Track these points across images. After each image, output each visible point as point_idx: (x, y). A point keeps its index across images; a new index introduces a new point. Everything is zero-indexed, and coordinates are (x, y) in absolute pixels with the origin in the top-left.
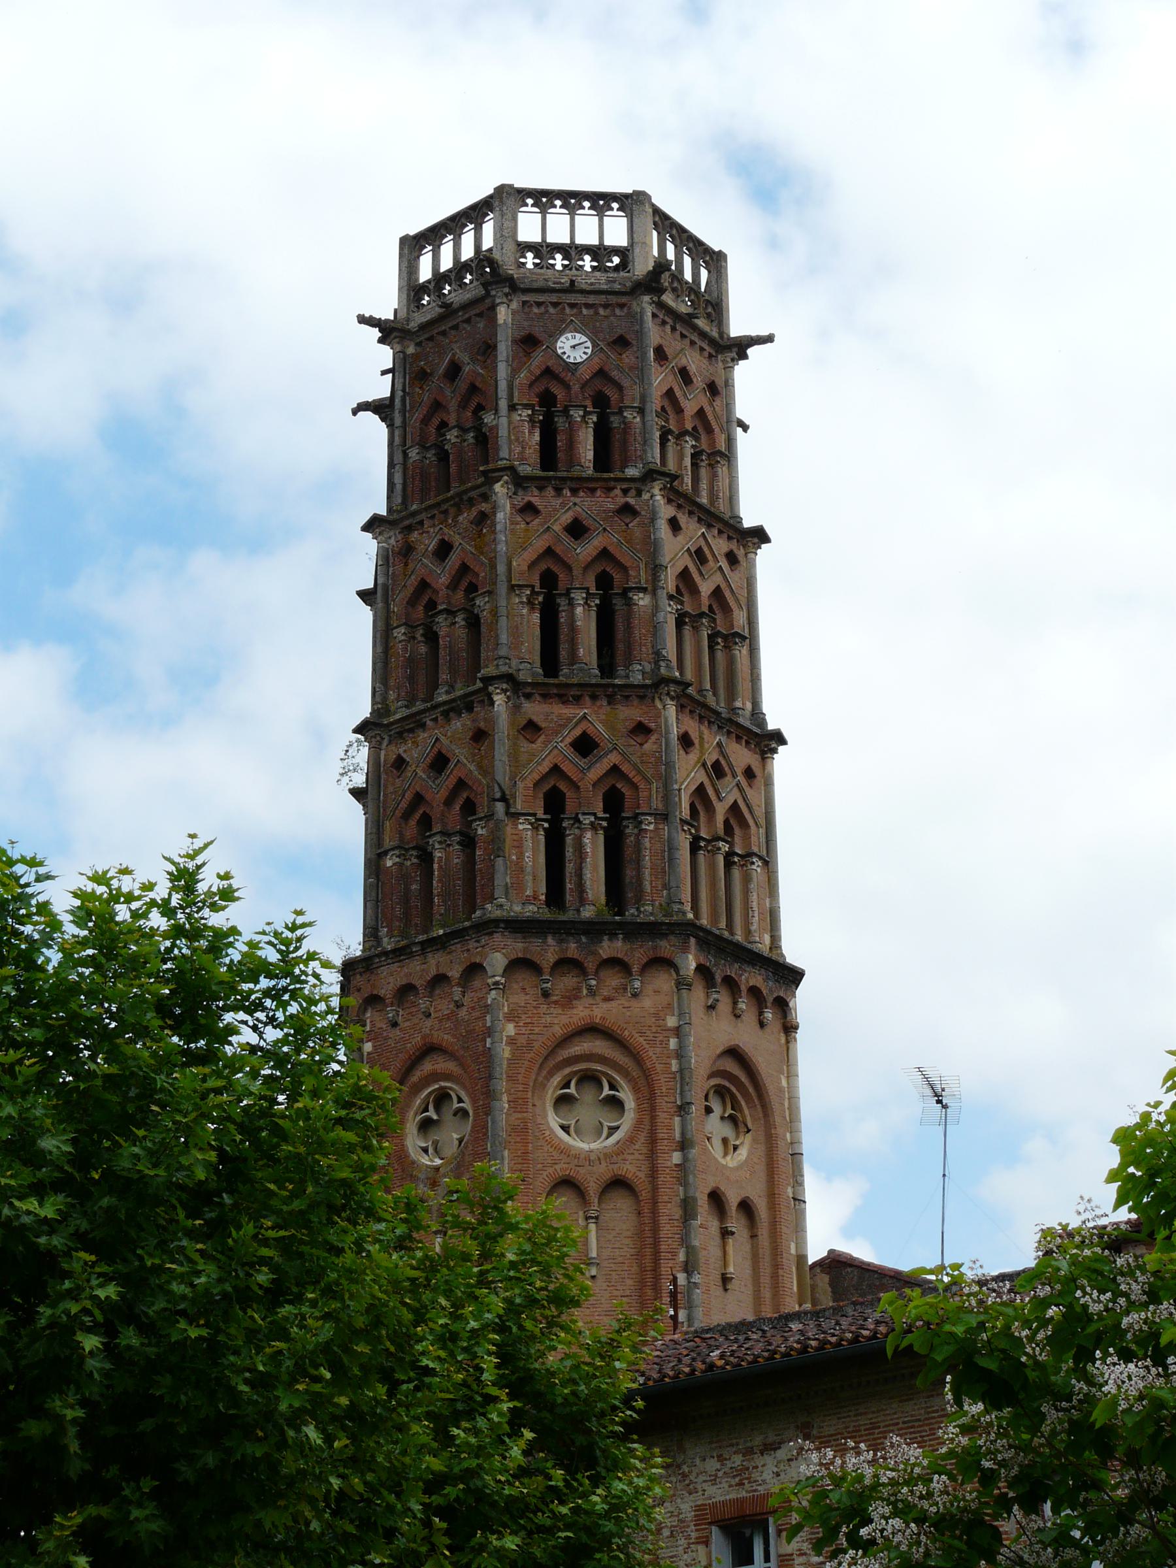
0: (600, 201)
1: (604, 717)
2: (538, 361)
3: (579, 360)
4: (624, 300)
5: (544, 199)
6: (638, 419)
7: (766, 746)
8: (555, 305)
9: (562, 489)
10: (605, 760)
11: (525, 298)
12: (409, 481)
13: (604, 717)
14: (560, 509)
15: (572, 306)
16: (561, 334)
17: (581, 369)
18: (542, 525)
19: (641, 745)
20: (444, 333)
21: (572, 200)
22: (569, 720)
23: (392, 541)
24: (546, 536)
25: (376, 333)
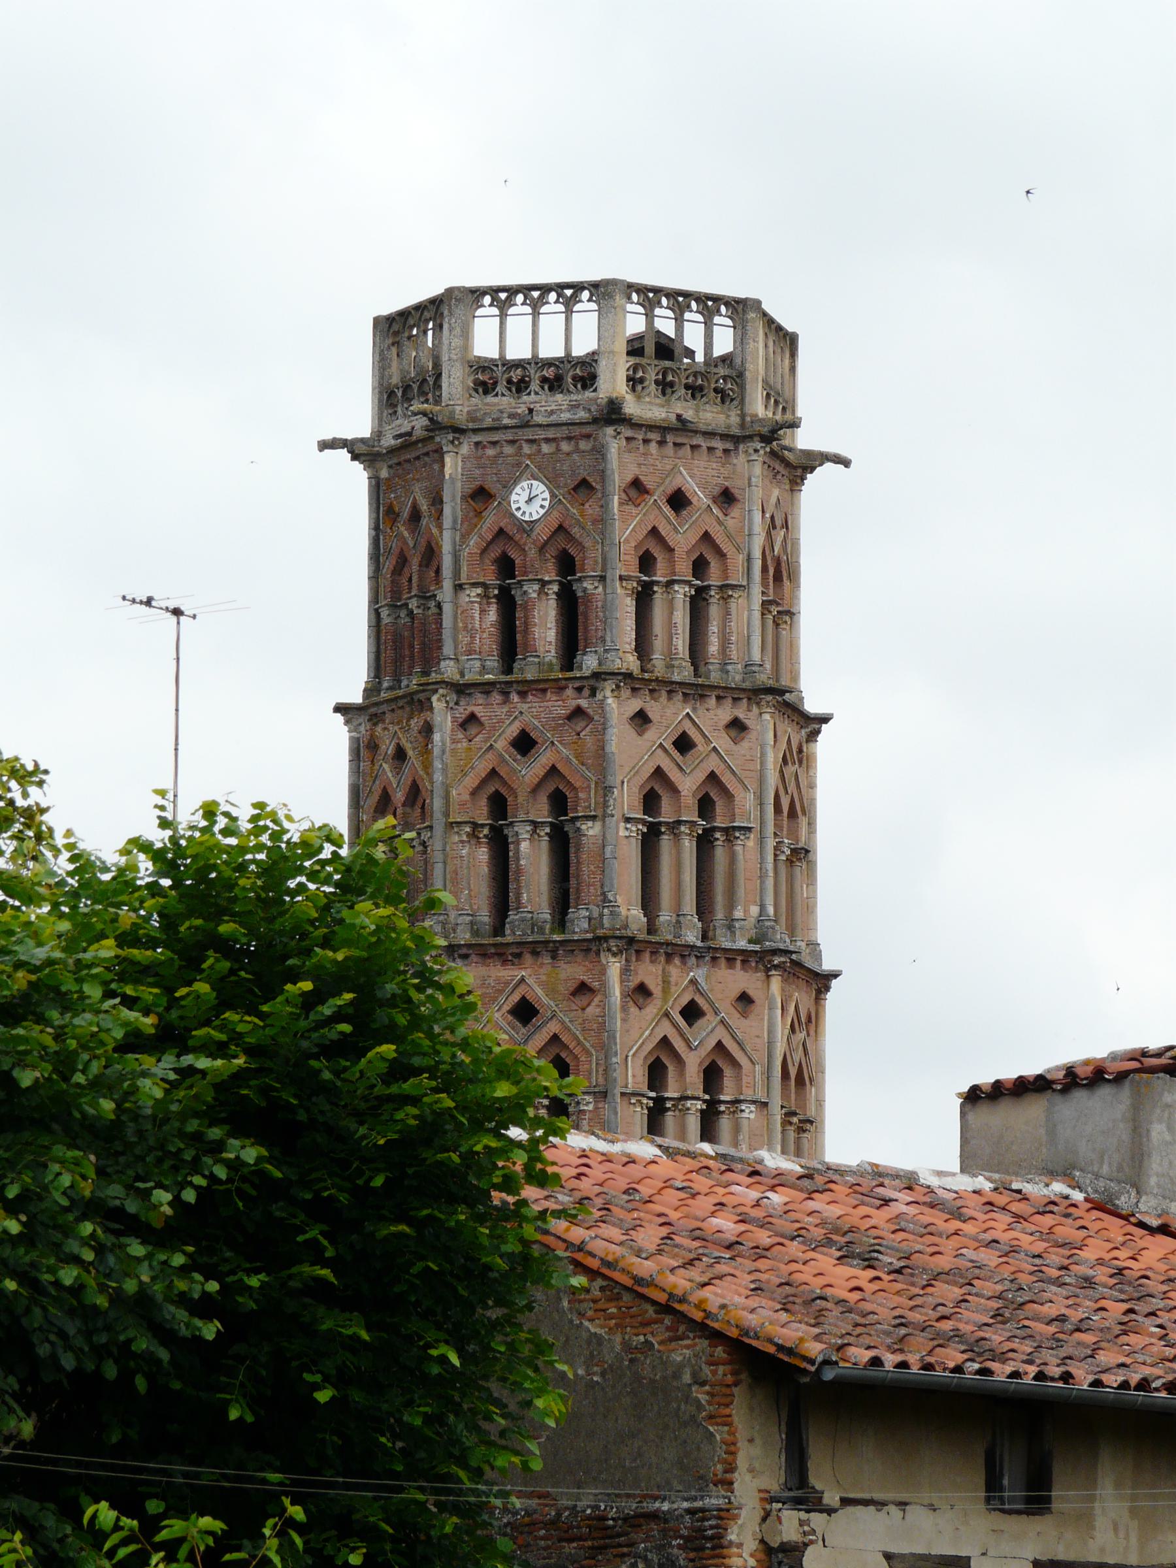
0: (569, 293)
1: (544, 978)
2: (490, 522)
3: (535, 517)
4: (587, 430)
5: (503, 297)
6: (600, 589)
7: (770, 961)
8: (512, 442)
9: (509, 693)
10: (545, 1030)
11: (477, 438)
12: (382, 647)
13: (544, 978)
14: (504, 719)
15: (531, 441)
16: (515, 483)
17: (538, 529)
18: (486, 741)
19: (583, 1009)
20: (408, 461)
21: (536, 294)
22: (507, 983)
23: (362, 729)
24: (489, 756)
25: (344, 454)
